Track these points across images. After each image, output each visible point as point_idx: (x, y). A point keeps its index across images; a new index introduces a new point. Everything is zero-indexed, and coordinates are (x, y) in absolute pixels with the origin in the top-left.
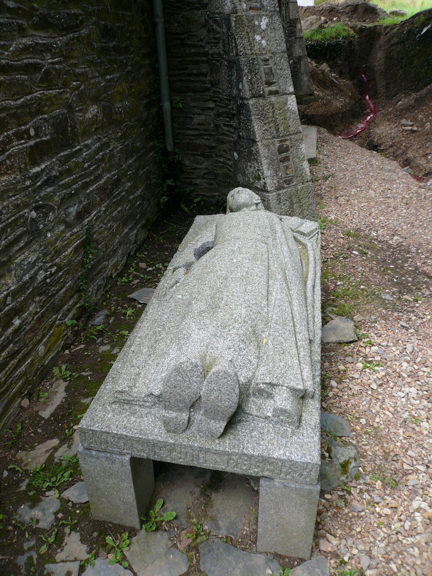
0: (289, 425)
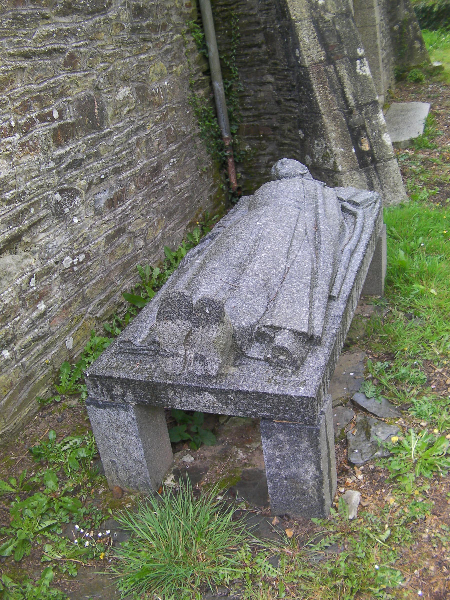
0: (290, 366)
